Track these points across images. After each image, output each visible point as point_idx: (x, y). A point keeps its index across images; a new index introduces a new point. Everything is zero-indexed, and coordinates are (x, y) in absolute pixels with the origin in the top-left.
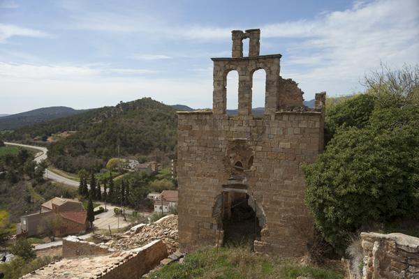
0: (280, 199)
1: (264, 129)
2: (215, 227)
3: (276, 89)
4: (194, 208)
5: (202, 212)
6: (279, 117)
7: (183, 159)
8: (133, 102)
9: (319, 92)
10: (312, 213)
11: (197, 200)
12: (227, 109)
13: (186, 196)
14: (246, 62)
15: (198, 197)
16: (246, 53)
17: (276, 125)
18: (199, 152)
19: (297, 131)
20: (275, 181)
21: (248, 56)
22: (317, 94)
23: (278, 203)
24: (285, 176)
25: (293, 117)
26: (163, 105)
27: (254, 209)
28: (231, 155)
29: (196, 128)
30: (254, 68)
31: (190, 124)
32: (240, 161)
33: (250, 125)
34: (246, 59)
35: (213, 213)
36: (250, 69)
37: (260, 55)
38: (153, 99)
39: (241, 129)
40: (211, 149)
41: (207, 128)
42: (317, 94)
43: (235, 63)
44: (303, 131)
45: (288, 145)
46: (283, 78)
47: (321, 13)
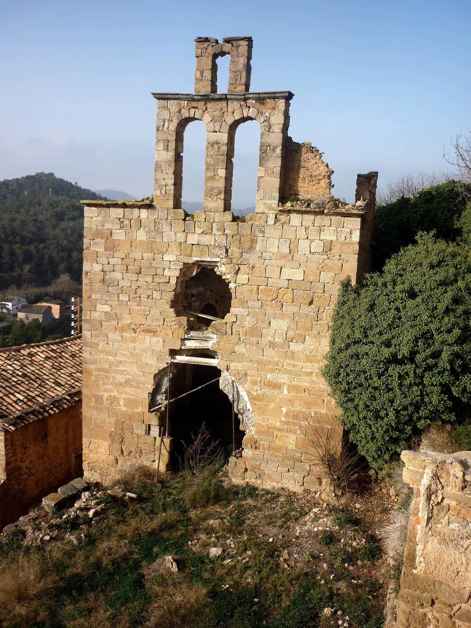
0: (283, 379)
1: (253, 242)
2: (155, 431)
3: (279, 162)
4: (115, 393)
5: (130, 403)
6: (283, 218)
7: (93, 297)
8: (17, 180)
9: (365, 172)
10: (340, 431)
11: (121, 378)
12: (360, 219)
13: (99, 370)
14: (224, 104)
15: (122, 372)
16: (223, 88)
17: (277, 233)
18: (125, 284)
19: (317, 246)
20: (272, 345)
21: (226, 92)
22: (359, 176)
23: (277, 386)
24: (291, 333)
25: (311, 217)
26: (78, 188)
27: (230, 397)
28: (194, 292)
29: (119, 235)
30: (237, 117)
31: (108, 226)
32: (212, 302)
33: (227, 232)
34: (225, 98)
35: (153, 403)
36: (230, 120)
37: (251, 91)
38: (58, 175)
39: (207, 240)
40: (149, 279)
41: (141, 235)
42: (359, 176)
43: (201, 104)
44: (329, 247)
45: (298, 276)
46: (294, 140)
47: (369, 235)
